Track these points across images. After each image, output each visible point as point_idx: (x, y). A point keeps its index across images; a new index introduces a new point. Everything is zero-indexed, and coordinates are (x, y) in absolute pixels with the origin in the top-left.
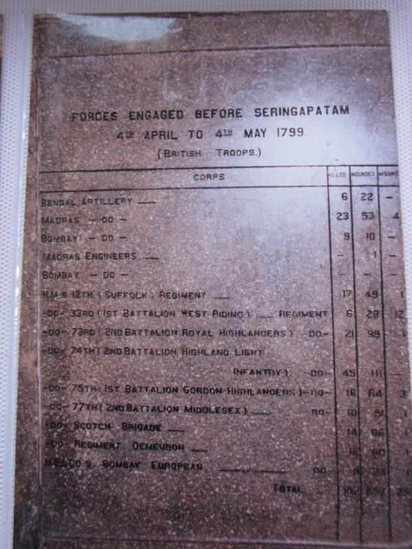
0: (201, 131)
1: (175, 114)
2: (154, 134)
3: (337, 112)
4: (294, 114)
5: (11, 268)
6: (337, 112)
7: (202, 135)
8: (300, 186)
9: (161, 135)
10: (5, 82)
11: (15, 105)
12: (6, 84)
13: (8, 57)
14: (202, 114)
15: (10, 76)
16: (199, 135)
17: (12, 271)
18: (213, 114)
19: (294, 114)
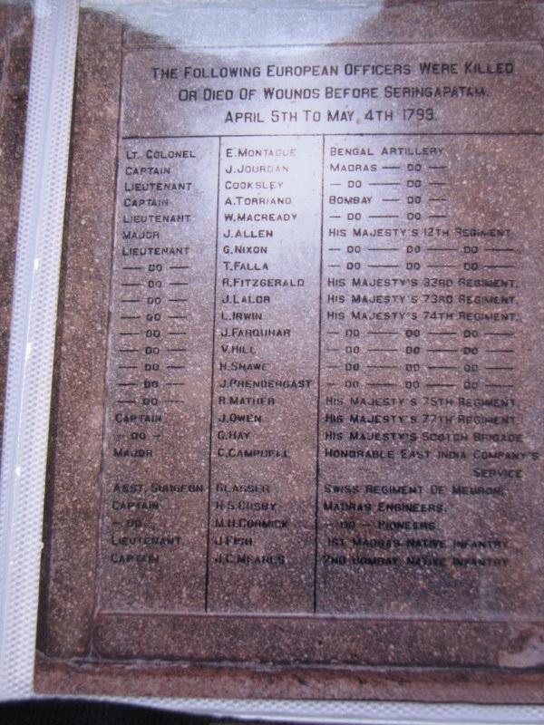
0: (319, 113)
1: (223, 94)
2: (239, 116)
3: (327, 73)
4: (256, 74)
5: (25, 292)
6: (327, 73)
7: (205, 94)
8: (362, 135)
9: (246, 118)
10: (28, 161)
11: (44, 59)
12: (29, 158)
13: (38, 49)
14: (334, 92)
15: (42, 52)
16: (317, 118)
17: (23, 326)
18: (345, 94)
19: (256, 74)
